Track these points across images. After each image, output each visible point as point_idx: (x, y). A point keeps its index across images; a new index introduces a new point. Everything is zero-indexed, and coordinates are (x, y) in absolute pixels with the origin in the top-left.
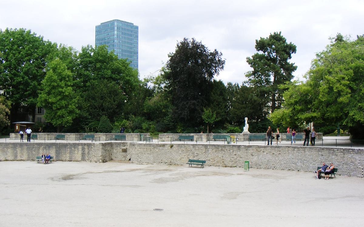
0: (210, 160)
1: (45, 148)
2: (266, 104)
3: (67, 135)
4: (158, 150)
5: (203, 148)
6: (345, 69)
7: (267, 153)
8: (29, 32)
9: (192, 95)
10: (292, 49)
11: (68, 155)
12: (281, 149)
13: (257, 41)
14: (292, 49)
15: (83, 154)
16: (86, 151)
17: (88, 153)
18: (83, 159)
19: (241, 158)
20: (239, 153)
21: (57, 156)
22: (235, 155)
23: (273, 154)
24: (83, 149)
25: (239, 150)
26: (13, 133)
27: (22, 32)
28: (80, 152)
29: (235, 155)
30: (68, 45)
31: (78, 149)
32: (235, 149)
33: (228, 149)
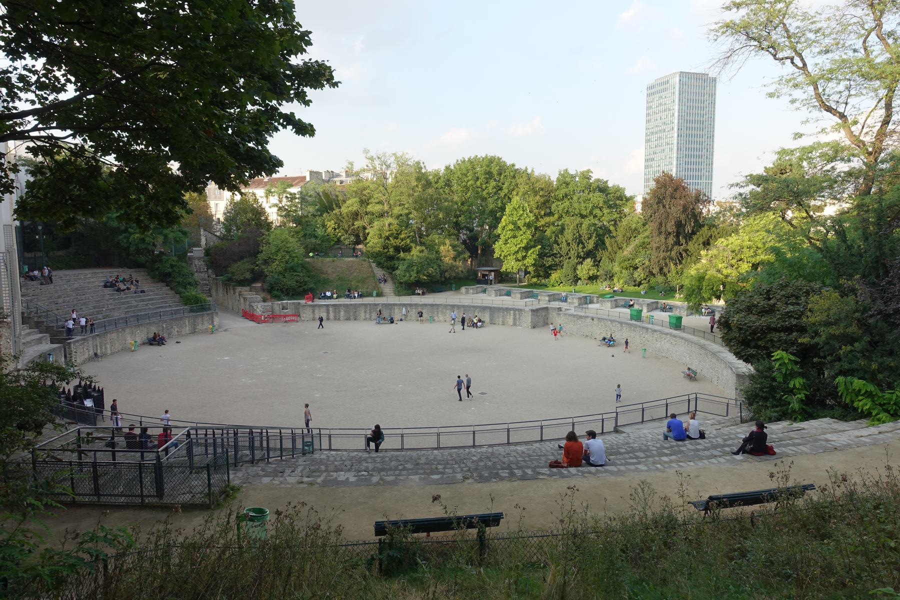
5: (619, 325)
6: (711, 237)
11: (501, 319)
15: (515, 319)
16: (518, 316)
18: (515, 324)
21: (491, 320)
24: (514, 315)
28: (512, 317)
32: (644, 331)
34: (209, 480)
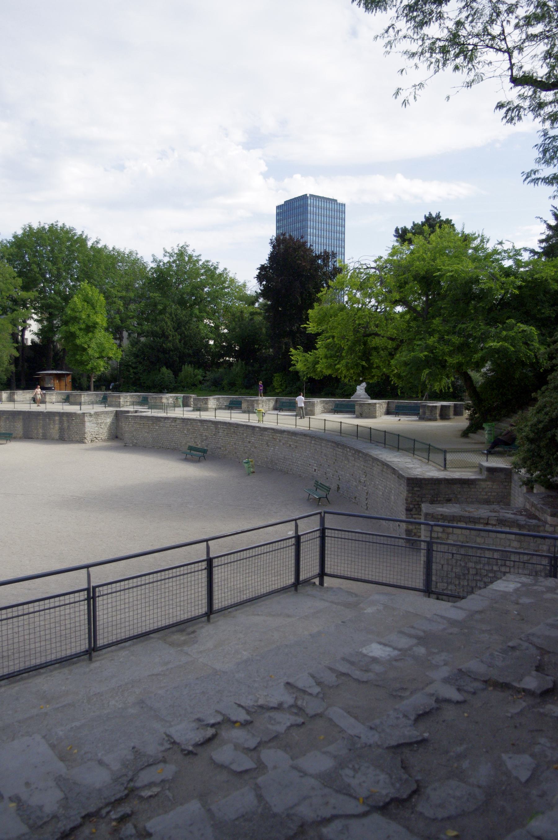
0: (220, 448)
1: (8, 418)
2: (451, 351)
3: (168, 398)
4: (157, 427)
7: (283, 444)
8: (52, 227)
9: (420, 339)
10: (451, 220)
11: (41, 431)
12: (298, 439)
13: (425, 216)
14: (451, 220)
16: (66, 424)
17: (69, 426)
19: (255, 447)
20: (253, 440)
22: (249, 442)
23: (290, 446)
24: (61, 422)
25: (253, 434)
26: (124, 394)
27: (52, 229)
28: (57, 427)
29: (249, 442)
30: (214, 261)
31: (54, 421)
33: (241, 432)
34: (440, 552)
